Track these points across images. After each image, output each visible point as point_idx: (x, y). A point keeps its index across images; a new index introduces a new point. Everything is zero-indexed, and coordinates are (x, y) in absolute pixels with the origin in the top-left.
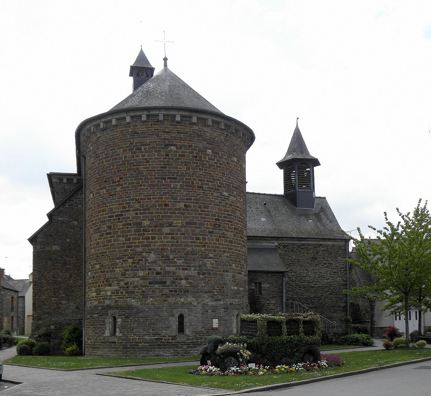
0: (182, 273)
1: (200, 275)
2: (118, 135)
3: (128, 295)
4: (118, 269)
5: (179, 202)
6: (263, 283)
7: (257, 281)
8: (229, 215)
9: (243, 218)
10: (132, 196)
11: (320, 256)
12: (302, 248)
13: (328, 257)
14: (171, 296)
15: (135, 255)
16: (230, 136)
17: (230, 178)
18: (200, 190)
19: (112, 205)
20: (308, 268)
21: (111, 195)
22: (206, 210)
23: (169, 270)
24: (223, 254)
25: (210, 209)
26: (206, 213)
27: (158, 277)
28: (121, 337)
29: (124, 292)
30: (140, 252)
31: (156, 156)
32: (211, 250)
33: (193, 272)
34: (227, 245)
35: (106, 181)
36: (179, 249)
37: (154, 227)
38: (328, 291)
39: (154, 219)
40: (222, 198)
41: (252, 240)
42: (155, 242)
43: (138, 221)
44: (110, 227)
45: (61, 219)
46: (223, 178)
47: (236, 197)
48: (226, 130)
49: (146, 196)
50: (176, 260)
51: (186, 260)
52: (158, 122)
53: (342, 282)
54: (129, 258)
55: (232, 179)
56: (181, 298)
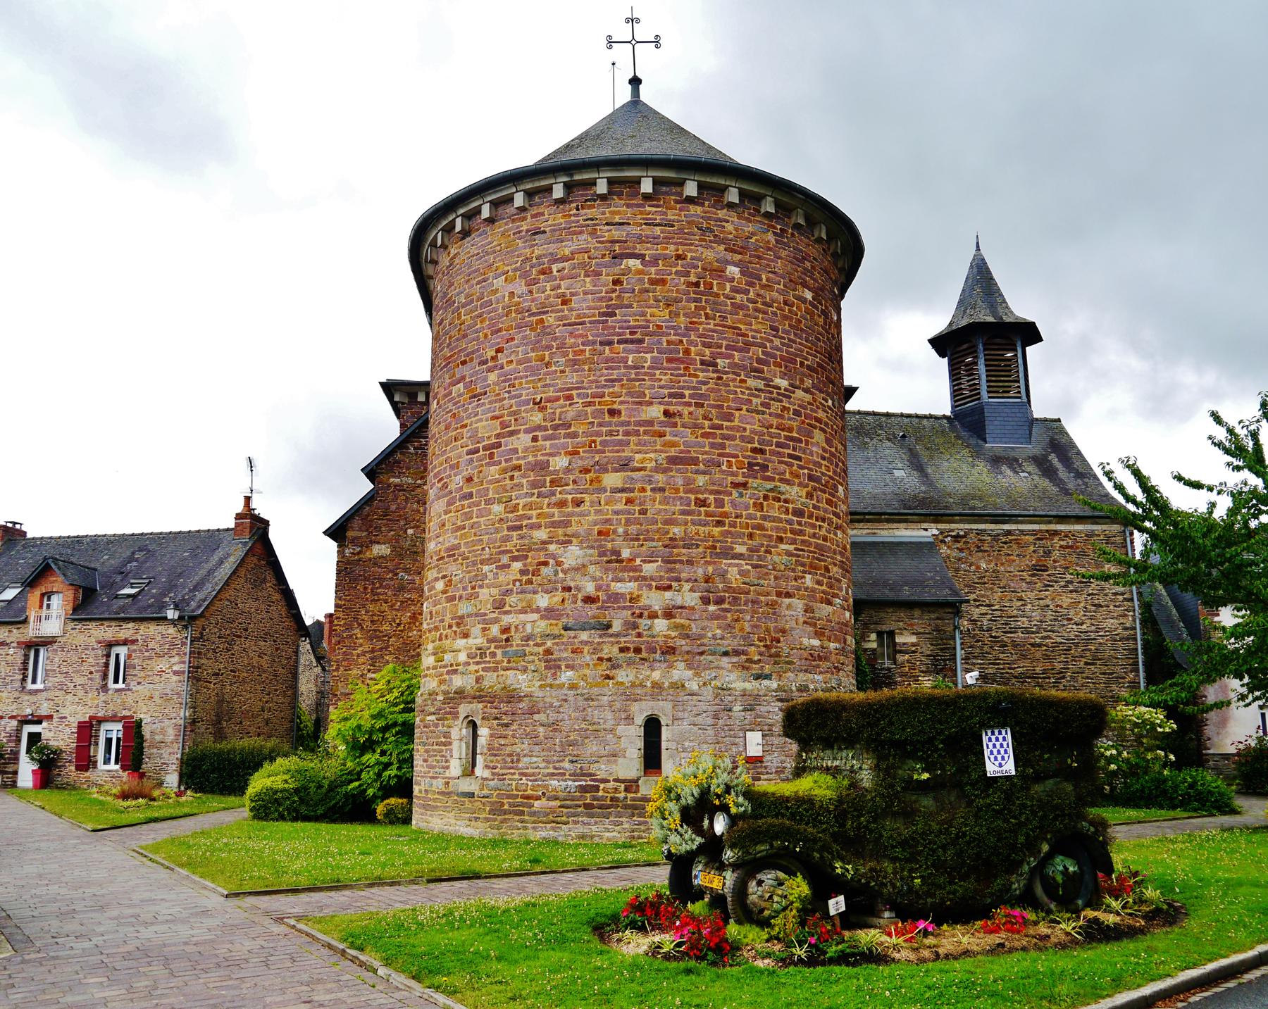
0: (655, 600)
1: (709, 603)
2: (495, 243)
3: (509, 662)
4: (485, 591)
5: (651, 404)
6: (902, 634)
7: (885, 628)
8: (792, 439)
9: (833, 450)
10: (524, 392)
11: (1055, 561)
12: (1005, 543)
13: (1077, 565)
14: (624, 665)
15: (530, 550)
16: (793, 235)
17: (794, 342)
18: (708, 371)
19: (477, 422)
20: (1023, 594)
21: (474, 397)
22: (725, 424)
23: (619, 591)
24: (777, 547)
25: (736, 423)
26: (725, 432)
27: (591, 610)
28: (486, 779)
29: (499, 652)
30: (544, 542)
31: (588, 285)
32: (741, 535)
33: (689, 598)
34: (789, 522)
35: (464, 363)
36: (648, 531)
37: (581, 472)
38: (1082, 657)
39: (581, 450)
40: (771, 393)
41: (869, 521)
42: (581, 514)
43: (540, 458)
44: (469, 480)
45: (397, 480)
46: (772, 341)
47: (812, 394)
48: (779, 218)
49: (561, 390)
50: (638, 561)
51: (669, 562)
52: (595, 201)
53: (1118, 631)
54: (514, 559)
55: (800, 344)
56: (653, 670)
